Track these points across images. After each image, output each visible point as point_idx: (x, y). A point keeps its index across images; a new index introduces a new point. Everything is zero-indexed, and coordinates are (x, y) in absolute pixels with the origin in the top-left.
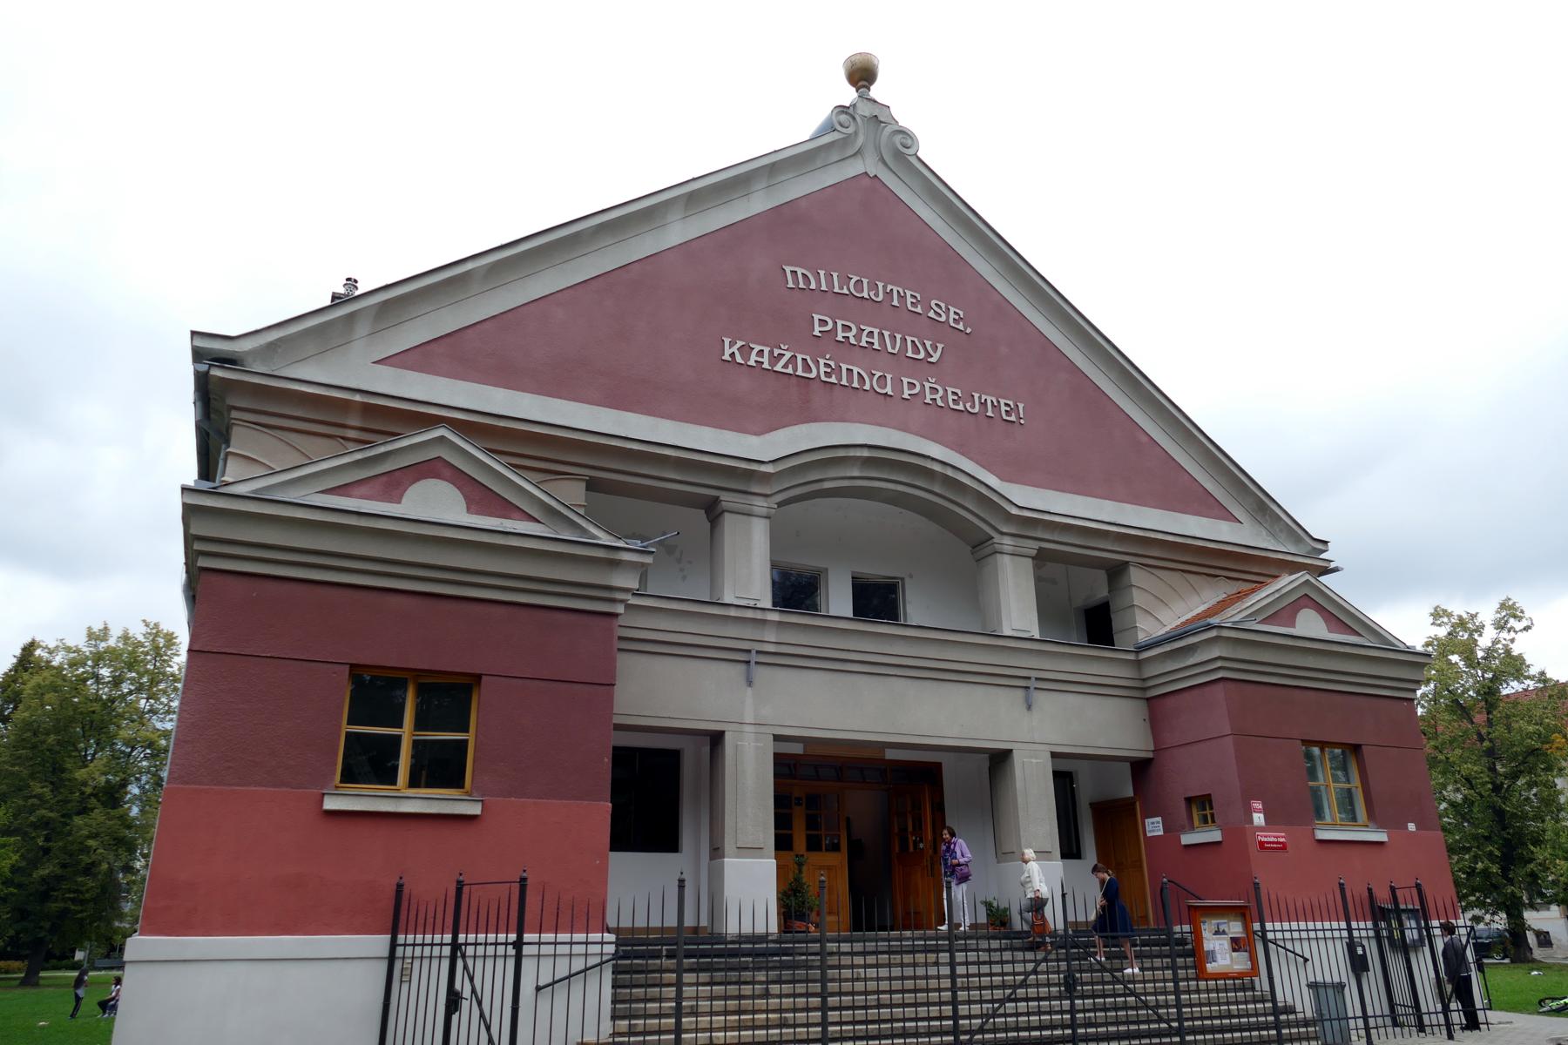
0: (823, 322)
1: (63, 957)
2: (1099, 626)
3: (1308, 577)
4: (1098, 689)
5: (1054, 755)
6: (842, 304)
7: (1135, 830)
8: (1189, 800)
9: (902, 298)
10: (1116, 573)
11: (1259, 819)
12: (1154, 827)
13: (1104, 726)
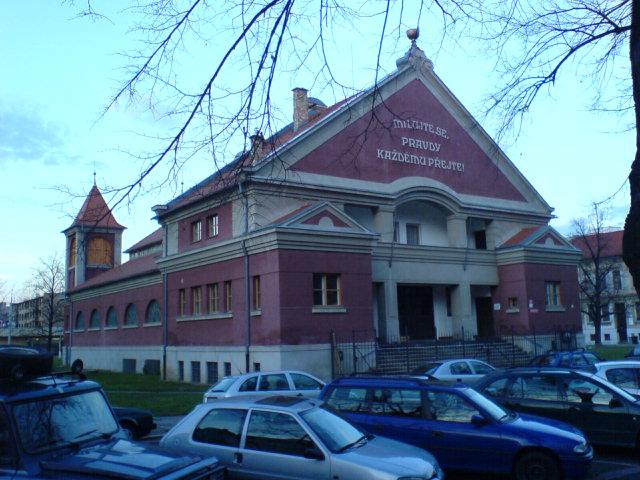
1: (539, 449)
2: (480, 240)
4: (483, 263)
6: (413, 133)
7: (491, 307)
10: (488, 222)
11: (531, 305)
12: (497, 307)
13: (486, 276)
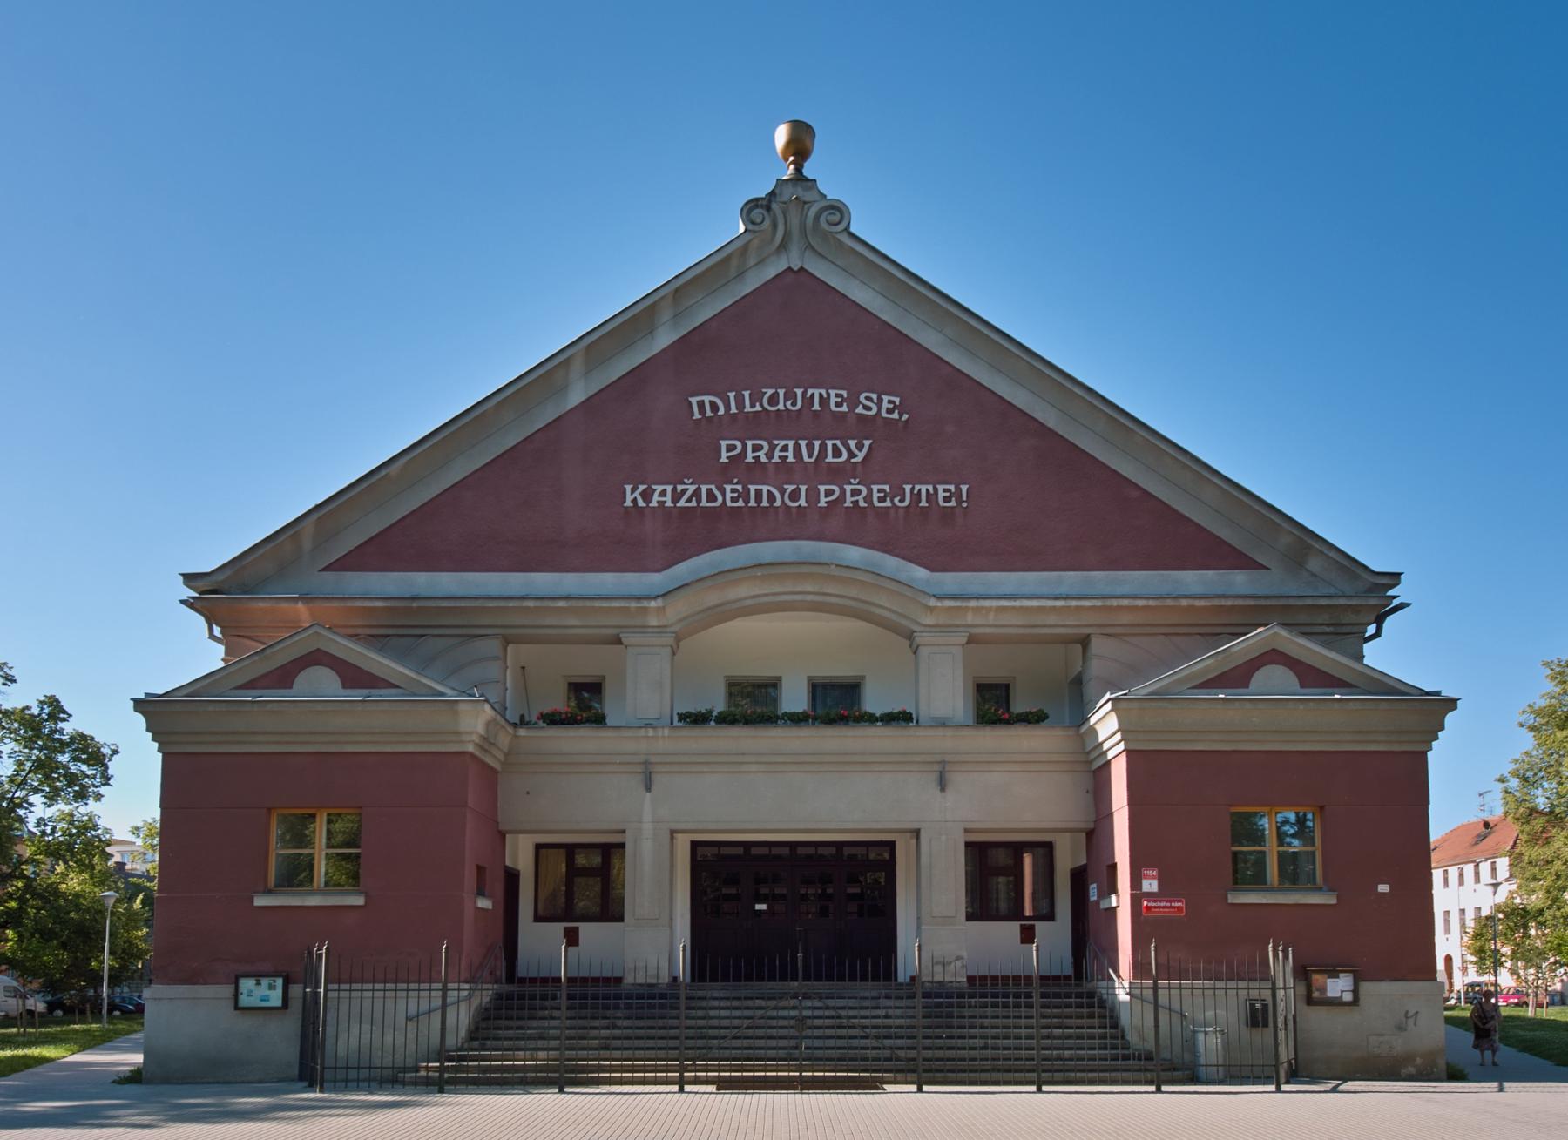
0: (730, 448)
6: (754, 425)
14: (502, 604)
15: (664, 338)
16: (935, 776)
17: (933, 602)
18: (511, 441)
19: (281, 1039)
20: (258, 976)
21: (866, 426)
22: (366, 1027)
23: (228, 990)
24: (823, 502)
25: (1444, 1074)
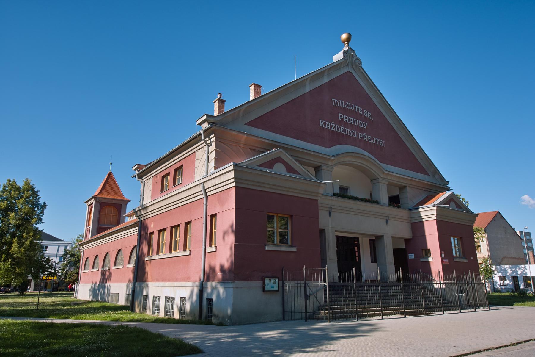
0: (341, 116)
3: (282, 150)
5: (392, 237)
6: (346, 111)
7: (406, 257)
8: (422, 250)
9: (358, 109)
14: (299, 149)
15: (326, 80)
16: (385, 220)
17: (385, 172)
18: (294, 97)
19: (274, 304)
20: (270, 278)
21: (365, 119)
22: (299, 298)
23: (259, 284)
24: (360, 137)
25: (486, 301)
